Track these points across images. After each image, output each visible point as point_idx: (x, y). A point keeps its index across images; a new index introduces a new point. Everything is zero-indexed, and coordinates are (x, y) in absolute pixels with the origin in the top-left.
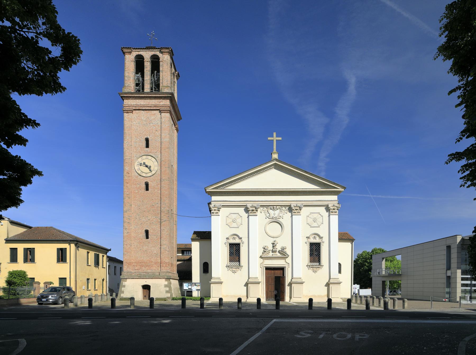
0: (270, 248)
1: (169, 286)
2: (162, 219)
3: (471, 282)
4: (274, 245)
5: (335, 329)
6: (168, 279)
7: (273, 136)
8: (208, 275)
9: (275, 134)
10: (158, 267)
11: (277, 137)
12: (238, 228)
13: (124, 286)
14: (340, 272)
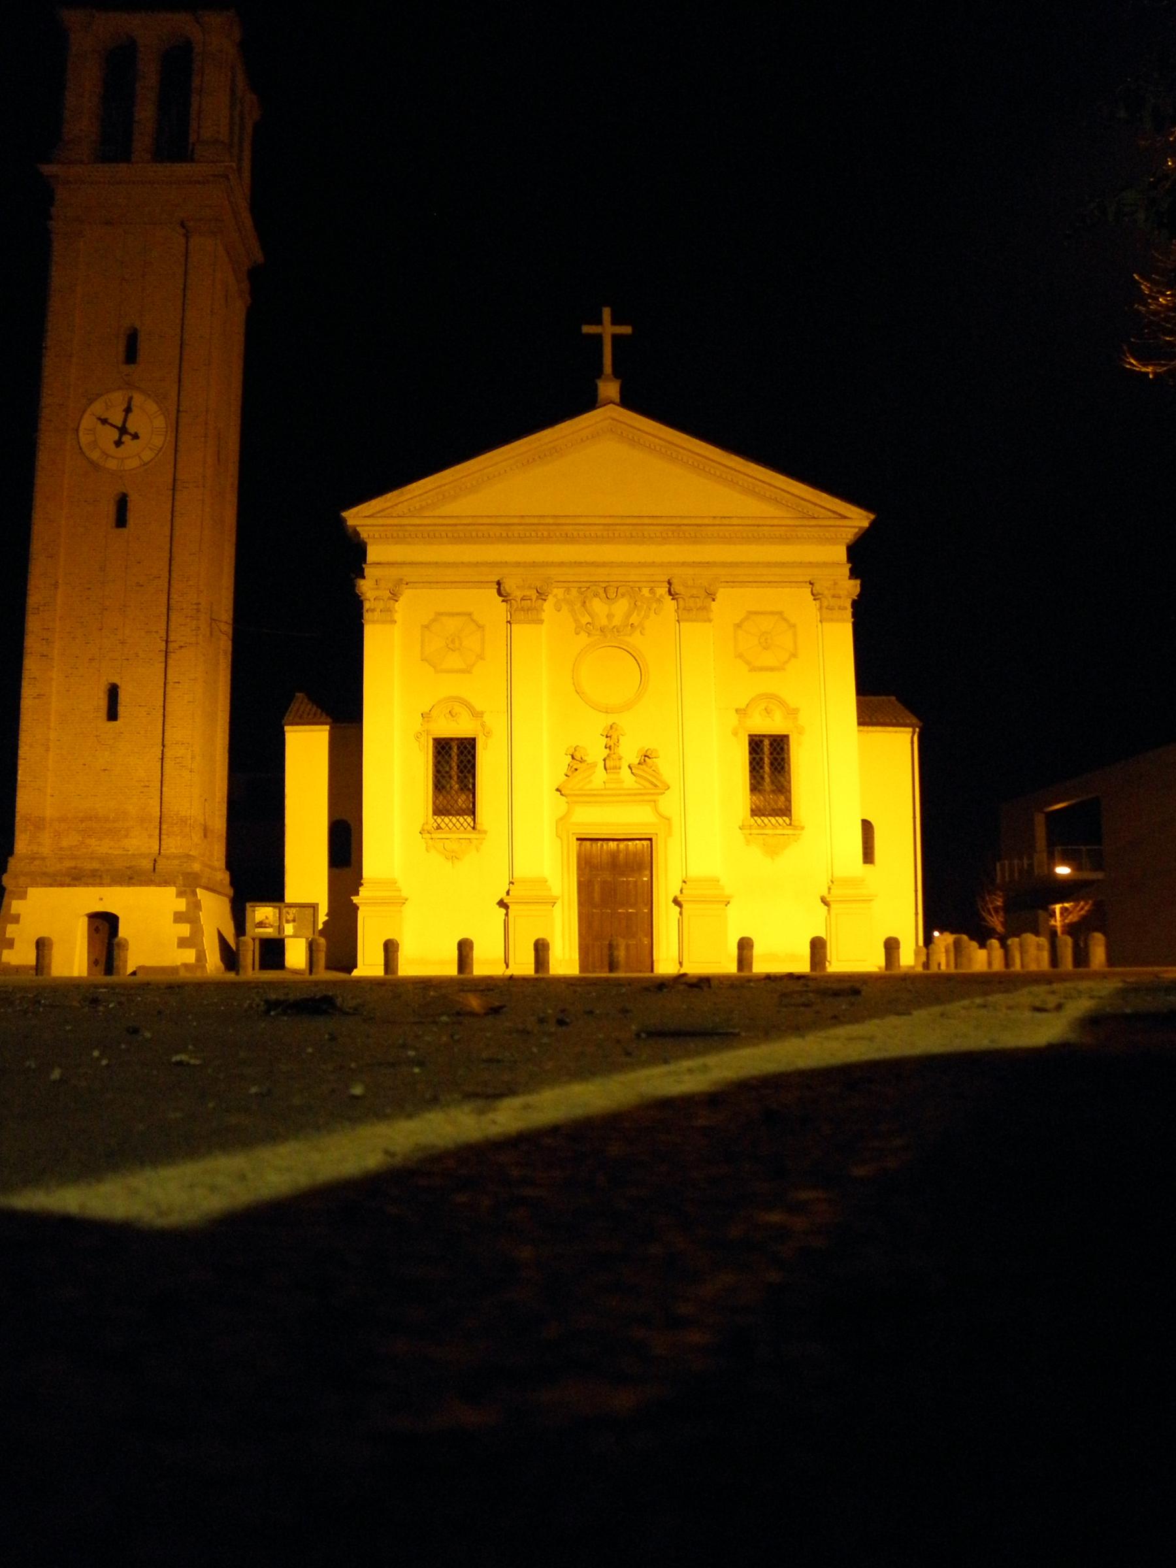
0: (596, 752)
1: (188, 917)
2: (171, 638)
3: (601, 910)
4: (611, 737)
5: (188, 856)
6: (188, 884)
7: (599, 321)
8: (337, 817)
9: (606, 313)
10: (150, 836)
11: (615, 337)
12: (469, 672)
13: (16, 919)
14: (868, 856)
